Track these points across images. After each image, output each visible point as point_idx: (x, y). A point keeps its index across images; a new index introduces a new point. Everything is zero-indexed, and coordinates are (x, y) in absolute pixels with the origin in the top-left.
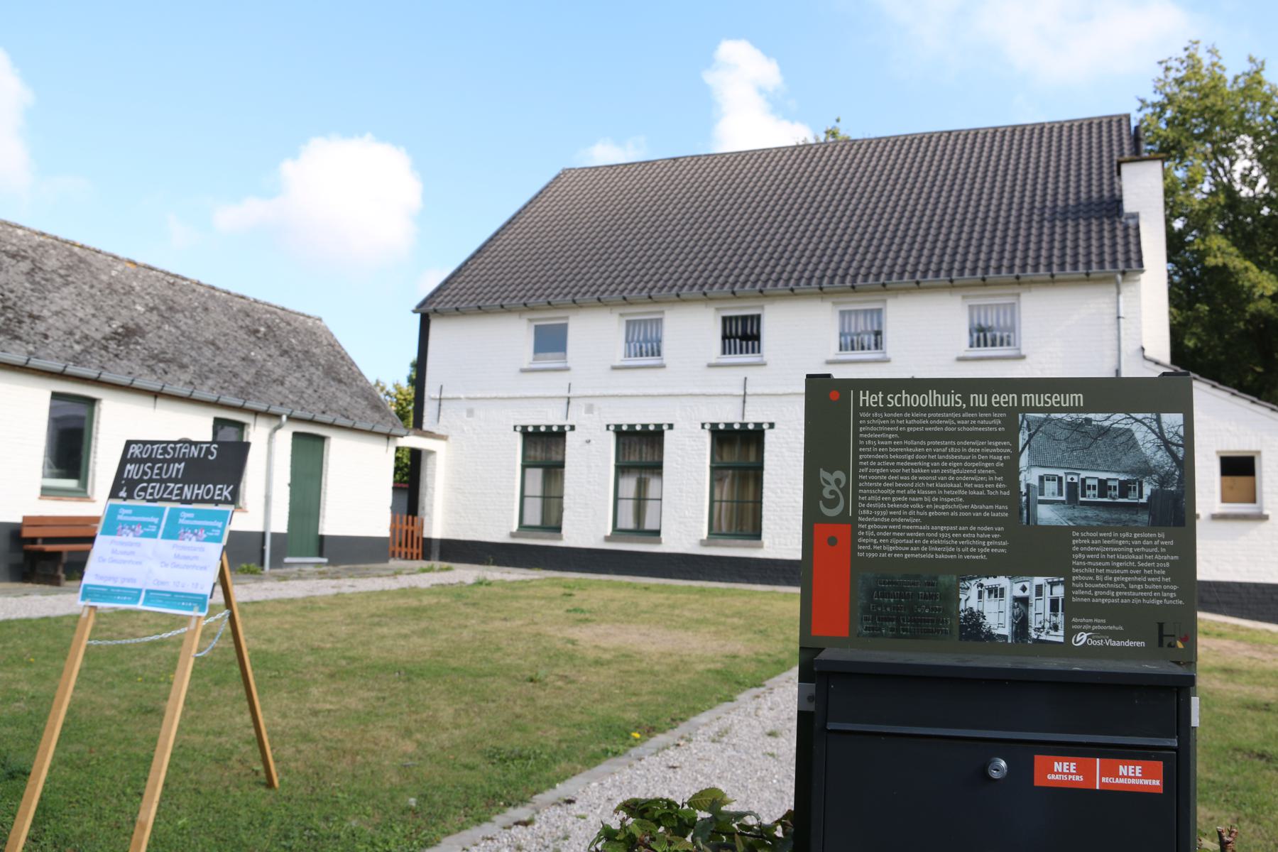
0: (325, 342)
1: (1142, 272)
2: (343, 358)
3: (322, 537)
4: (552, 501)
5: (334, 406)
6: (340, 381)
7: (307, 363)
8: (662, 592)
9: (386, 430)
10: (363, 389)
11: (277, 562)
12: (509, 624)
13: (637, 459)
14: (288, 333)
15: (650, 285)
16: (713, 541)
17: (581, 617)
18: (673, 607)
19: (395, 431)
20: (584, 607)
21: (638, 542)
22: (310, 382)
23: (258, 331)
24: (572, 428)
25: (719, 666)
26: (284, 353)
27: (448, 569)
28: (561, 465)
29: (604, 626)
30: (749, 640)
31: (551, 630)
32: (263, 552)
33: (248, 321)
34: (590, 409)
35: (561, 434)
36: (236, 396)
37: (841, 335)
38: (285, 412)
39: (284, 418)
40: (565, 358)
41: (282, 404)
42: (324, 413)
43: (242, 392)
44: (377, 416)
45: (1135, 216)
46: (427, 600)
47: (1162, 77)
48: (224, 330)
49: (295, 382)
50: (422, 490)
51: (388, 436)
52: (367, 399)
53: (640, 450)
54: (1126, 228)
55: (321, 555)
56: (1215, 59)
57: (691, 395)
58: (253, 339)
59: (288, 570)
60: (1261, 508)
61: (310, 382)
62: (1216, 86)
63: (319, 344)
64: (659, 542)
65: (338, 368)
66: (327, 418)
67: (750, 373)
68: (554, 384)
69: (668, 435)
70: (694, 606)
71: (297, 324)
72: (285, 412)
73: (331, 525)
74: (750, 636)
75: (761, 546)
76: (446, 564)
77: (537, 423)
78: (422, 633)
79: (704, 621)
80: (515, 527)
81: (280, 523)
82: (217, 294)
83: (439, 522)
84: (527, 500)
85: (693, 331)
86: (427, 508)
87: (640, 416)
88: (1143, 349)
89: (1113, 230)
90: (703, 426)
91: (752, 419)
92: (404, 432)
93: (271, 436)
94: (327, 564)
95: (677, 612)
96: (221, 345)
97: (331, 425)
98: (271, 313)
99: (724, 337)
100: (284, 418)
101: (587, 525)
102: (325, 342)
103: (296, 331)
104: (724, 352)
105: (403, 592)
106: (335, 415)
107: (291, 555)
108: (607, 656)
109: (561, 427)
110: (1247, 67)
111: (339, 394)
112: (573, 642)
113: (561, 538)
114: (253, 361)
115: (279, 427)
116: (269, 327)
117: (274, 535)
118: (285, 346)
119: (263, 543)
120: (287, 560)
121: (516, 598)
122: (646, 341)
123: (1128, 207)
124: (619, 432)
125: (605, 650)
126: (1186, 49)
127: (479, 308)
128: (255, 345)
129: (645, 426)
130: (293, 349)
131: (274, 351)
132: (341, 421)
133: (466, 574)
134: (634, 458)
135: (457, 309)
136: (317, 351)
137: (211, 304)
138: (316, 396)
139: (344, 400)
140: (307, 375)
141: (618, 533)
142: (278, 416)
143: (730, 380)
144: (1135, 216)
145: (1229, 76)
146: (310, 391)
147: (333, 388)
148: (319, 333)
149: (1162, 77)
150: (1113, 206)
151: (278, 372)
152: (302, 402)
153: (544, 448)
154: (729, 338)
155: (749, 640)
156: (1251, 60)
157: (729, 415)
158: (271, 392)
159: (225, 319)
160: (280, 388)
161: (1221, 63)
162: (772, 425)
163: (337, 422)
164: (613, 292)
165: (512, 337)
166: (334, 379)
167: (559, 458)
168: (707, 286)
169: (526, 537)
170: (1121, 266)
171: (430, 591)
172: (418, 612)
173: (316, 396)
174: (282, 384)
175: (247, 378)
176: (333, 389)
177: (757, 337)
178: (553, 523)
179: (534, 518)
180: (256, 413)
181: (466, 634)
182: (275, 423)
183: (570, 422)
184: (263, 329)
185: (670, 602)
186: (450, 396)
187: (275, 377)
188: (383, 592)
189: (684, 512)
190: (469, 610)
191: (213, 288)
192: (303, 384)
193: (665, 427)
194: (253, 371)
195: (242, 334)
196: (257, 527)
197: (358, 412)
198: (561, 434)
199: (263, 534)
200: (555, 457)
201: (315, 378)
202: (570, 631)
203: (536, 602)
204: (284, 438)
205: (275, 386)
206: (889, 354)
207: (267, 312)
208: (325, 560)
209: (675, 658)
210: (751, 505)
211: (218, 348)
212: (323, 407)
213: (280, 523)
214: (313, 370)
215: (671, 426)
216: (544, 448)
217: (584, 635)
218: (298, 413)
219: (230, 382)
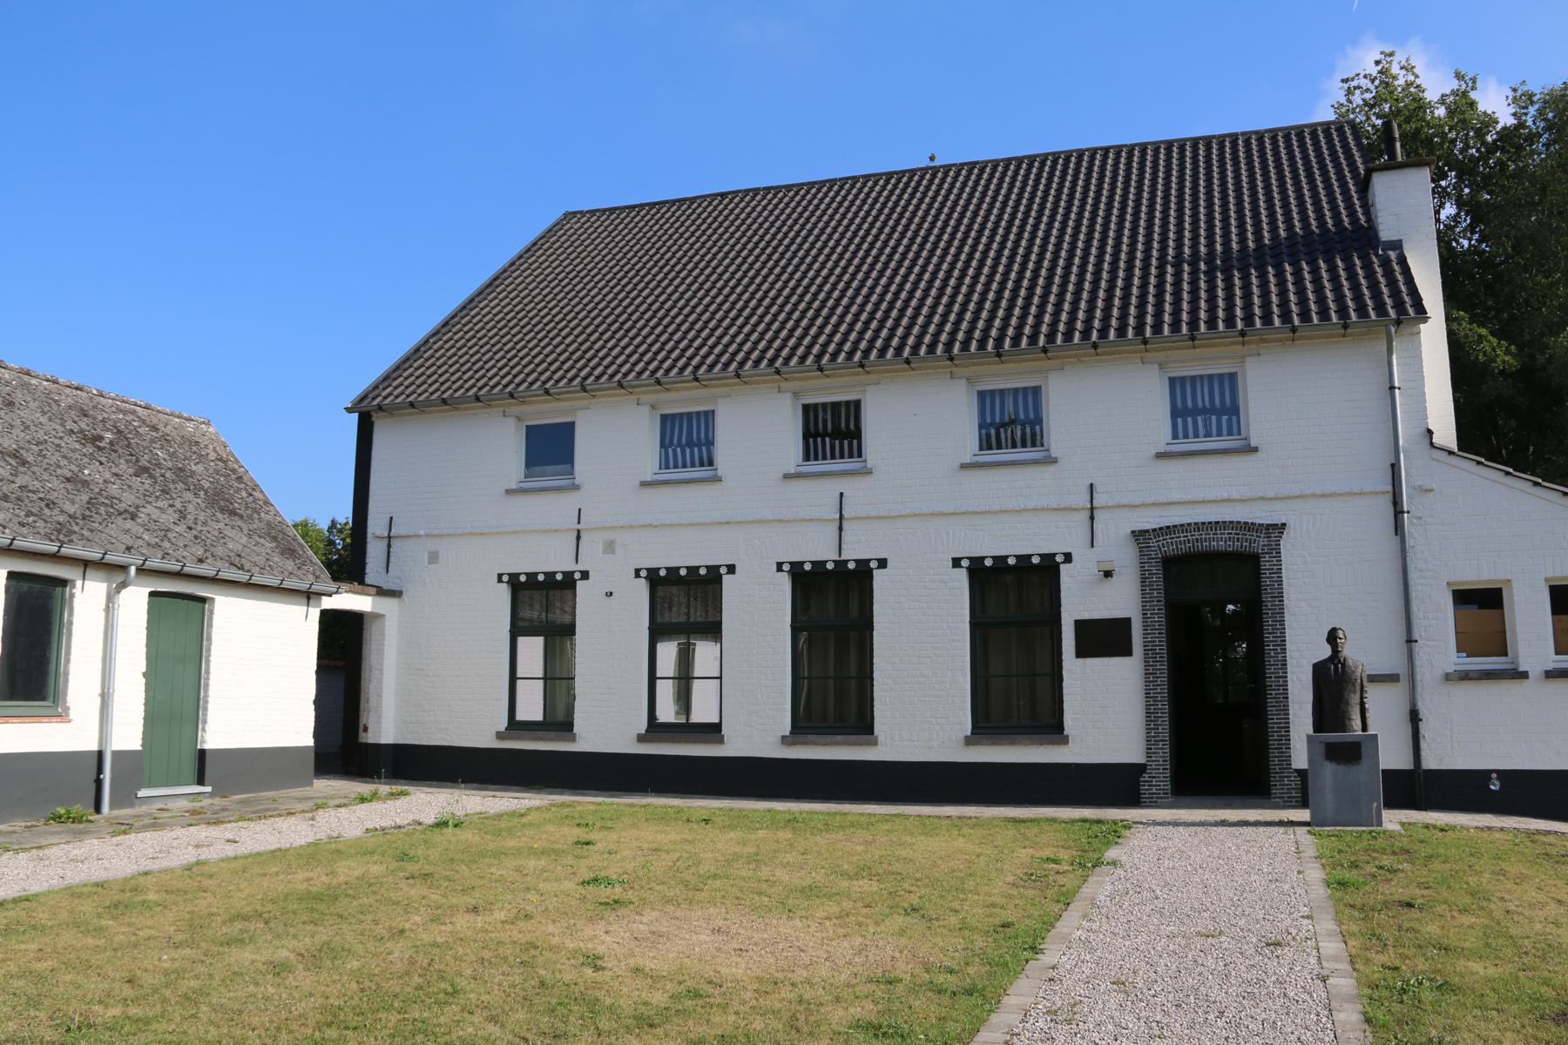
0: (213, 456)
1: (1425, 320)
2: (239, 479)
3: (202, 753)
4: (558, 679)
5: (220, 551)
6: (233, 513)
7: (180, 486)
8: (732, 827)
9: (304, 586)
10: (269, 524)
11: (125, 796)
12: (479, 921)
13: (682, 619)
14: (152, 441)
15: (695, 362)
16: (800, 738)
17: (608, 897)
18: (755, 860)
19: (316, 588)
20: (613, 873)
21: (687, 741)
22: (183, 515)
23: (101, 438)
24: (585, 575)
25: (866, 1011)
26: (142, 471)
27: (402, 794)
28: (570, 630)
29: (649, 915)
30: (902, 932)
31: (550, 931)
32: (99, 783)
33: (84, 424)
34: (610, 547)
35: (568, 583)
36: (48, 537)
37: (981, 427)
38: (134, 561)
39: (133, 569)
40: (572, 473)
41: (129, 549)
42: (201, 561)
43: (62, 532)
44: (290, 565)
45: (1397, 245)
46: (348, 870)
47: (1343, 100)
48: (41, 435)
49: (156, 514)
50: (365, 674)
51: (309, 596)
52: (275, 539)
53: (685, 604)
54: (1386, 263)
55: (201, 782)
56: (1411, 78)
57: (760, 522)
58: (90, 449)
59: (144, 809)
60: (1515, 662)
61: (183, 515)
62: (1420, 106)
63: (202, 459)
64: (721, 741)
65: (231, 495)
66: (206, 570)
67: (850, 487)
68: (554, 509)
69: (879, 577)
70: (789, 858)
71: (168, 430)
72: (134, 561)
73: (218, 734)
74: (899, 920)
75: (875, 743)
76: (397, 788)
77: (1047, 549)
78: (313, 959)
79: (809, 892)
80: (502, 724)
81: (128, 735)
82: (34, 381)
83: (386, 724)
84: (519, 683)
85: (758, 429)
86: (373, 700)
87: (684, 552)
88: (1430, 432)
89: (1367, 266)
90: (956, 563)
91: (854, 551)
92: (332, 586)
93: (110, 599)
94: (211, 795)
95: (765, 872)
96: (31, 459)
97: (214, 581)
98: (125, 412)
99: (1175, 413)
100: (133, 569)
101: (607, 723)
102: (213, 456)
103: (165, 439)
104: (807, 457)
105: (311, 854)
106: (219, 564)
107: (149, 786)
108: (659, 998)
109: (568, 575)
110: (1454, 84)
111: (228, 532)
112: (595, 962)
113: (573, 739)
114: (85, 483)
115: (124, 585)
116: (119, 432)
117: (117, 755)
118: (143, 463)
119: (100, 770)
120: (142, 793)
121: (499, 854)
122: (690, 444)
123: (1385, 235)
124: (977, 571)
125: (655, 979)
126: (1377, 63)
127: (444, 401)
128: (92, 457)
129: (693, 570)
130: (159, 465)
131: (123, 467)
132: (229, 574)
133: (426, 803)
134: (677, 616)
135: (412, 405)
136: (199, 469)
137: (18, 397)
138: (190, 535)
139: (237, 540)
140: (178, 505)
141: (656, 729)
142: (123, 568)
143: (818, 496)
144: (1397, 245)
145: (1431, 95)
146: (181, 528)
147: (222, 522)
148: (204, 441)
149: (1343, 100)
150: (1361, 240)
151: (128, 499)
152: (166, 544)
153: (542, 605)
154: (816, 435)
155: (902, 932)
156: (1459, 76)
157: (818, 548)
158: (113, 530)
159: (43, 420)
160: (129, 524)
161: (1418, 81)
162: (883, 563)
163: (222, 575)
164: (640, 373)
165: (499, 443)
166: (222, 510)
167: (567, 619)
168: (780, 360)
169: (520, 738)
170: (1392, 313)
171: (361, 849)
172: (320, 903)
173: (190, 535)
174: (133, 517)
175: (71, 509)
176: (221, 525)
177: (855, 434)
178: (560, 717)
179: (531, 707)
180: (86, 564)
181: (399, 951)
182: (121, 579)
183: (581, 567)
184: (108, 435)
185: (750, 849)
186: (404, 532)
187: (122, 506)
188: (277, 854)
189: (748, 690)
190: (416, 891)
191: (28, 373)
192: (169, 517)
193: (723, 570)
194: (85, 498)
195: (72, 442)
196: (87, 742)
197: (261, 560)
198: (568, 583)
199: (100, 755)
200: (558, 617)
201: (191, 508)
202: (588, 931)
203: (532, 864)
204: (135, 599)
205: (119, 520)
206: (1054, 452)
207: (119, 410)
208: (208, 789)
209: (786, 993)
210: (853, 683)
211: (24, 463)
212: (200, 553)
213: (128, 735)
214: (188, 496)
215: (731, 569)
216: (542, 605)
217: (608, 937)
218: (155, 563)
219: (39, 515)
